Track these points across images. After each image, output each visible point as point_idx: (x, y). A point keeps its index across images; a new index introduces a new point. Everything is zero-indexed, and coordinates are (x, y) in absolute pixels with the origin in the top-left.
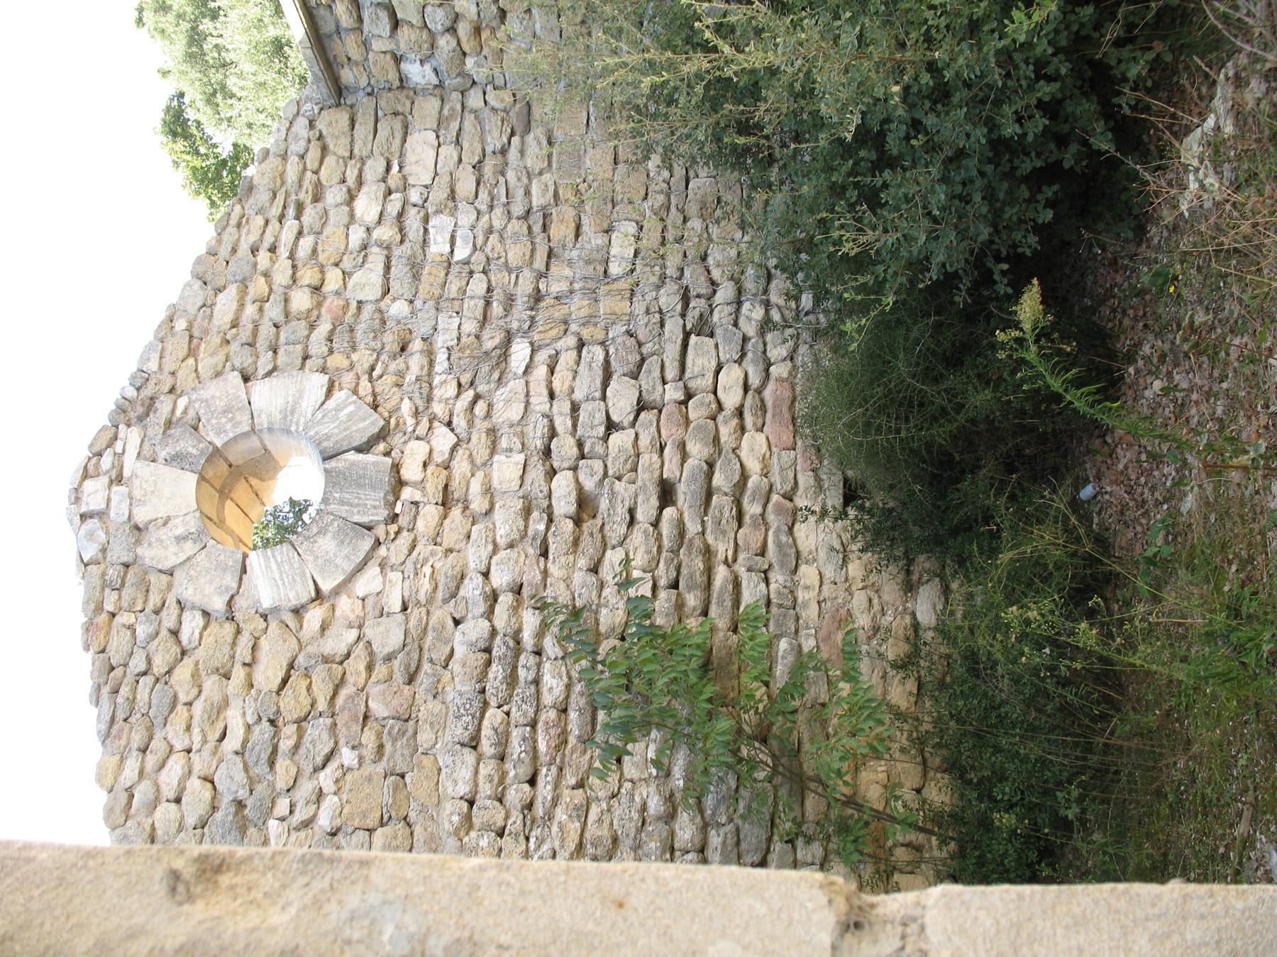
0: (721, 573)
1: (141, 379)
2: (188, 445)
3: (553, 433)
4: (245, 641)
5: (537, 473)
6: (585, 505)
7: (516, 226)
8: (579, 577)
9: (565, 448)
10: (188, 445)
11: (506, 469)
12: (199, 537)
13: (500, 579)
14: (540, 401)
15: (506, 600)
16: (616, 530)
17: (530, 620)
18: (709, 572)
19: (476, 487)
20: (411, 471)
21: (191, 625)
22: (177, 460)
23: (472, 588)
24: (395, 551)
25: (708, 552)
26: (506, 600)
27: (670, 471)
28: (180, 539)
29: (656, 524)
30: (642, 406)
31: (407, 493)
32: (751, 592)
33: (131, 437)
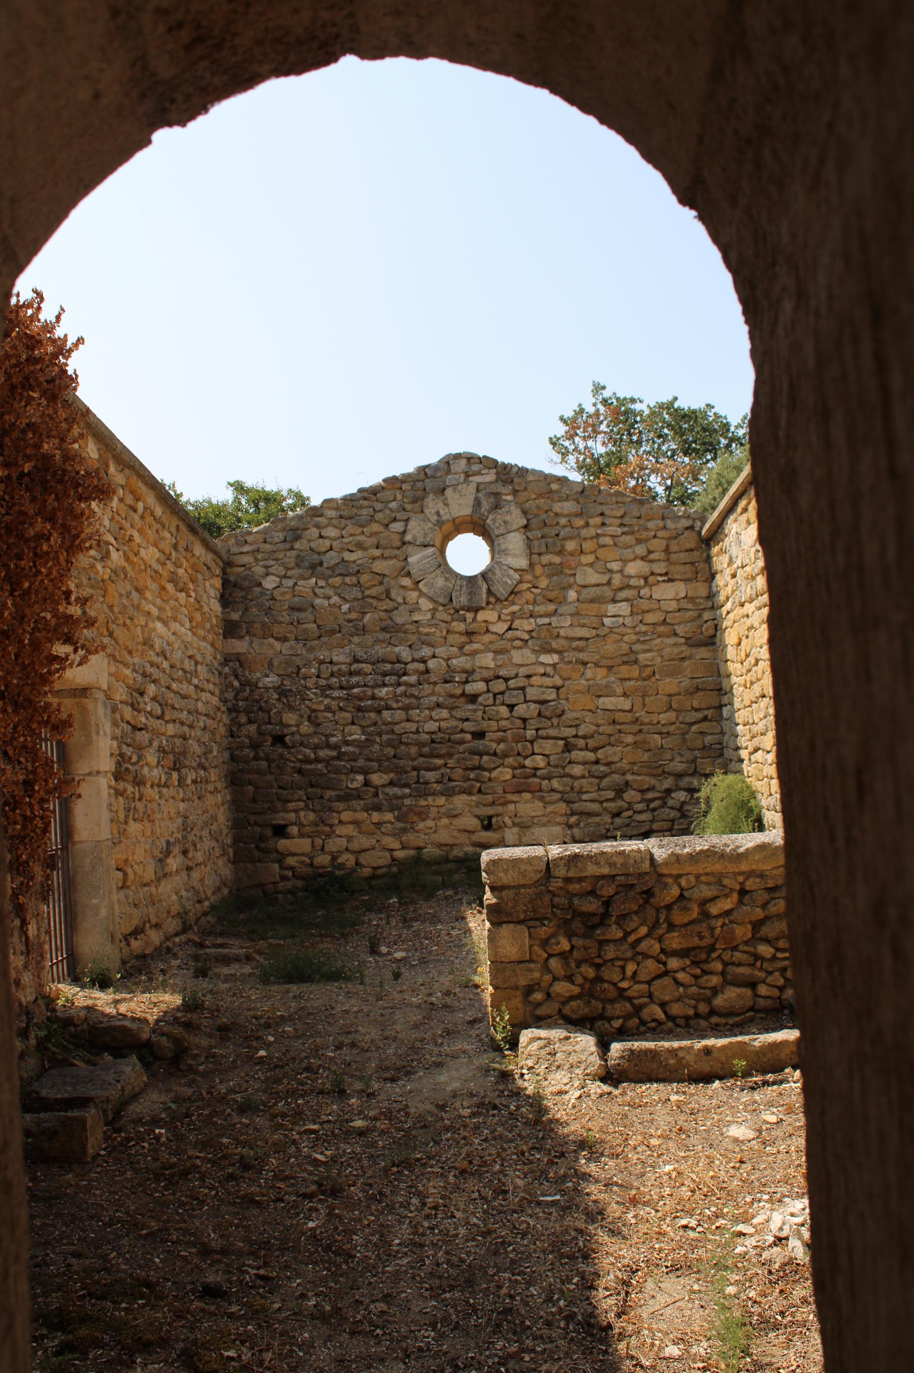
0: (440, 762)
1: (523, 472)
2: (485, 506)
3: (506, 680)
4: (396, 552)
5: (486, 674)
6: (473, 698)
7: (625, 647)
8: (434, 699)
9: (499, 686)
10: (485, 506)
11: (487, 660)
12: (440, 523)
13: (431, 664)
14: (523, 671)
15: (421, 667)
16: (458, 714)
17: (413, 679)
18: (439, 756)
19: (476, 646)
20: (481, 616)
21: (398, 527)
22: (477, 503)
23: (426, 651)
24: (442, 615)
25: (450, 755)
26: (421, 667)
27: (489, 736)
28: (438, 513)
29: (462, 731)
30: (524, 720)
31: (469, 616)
32: (430, 776)
33: (490, 476)
